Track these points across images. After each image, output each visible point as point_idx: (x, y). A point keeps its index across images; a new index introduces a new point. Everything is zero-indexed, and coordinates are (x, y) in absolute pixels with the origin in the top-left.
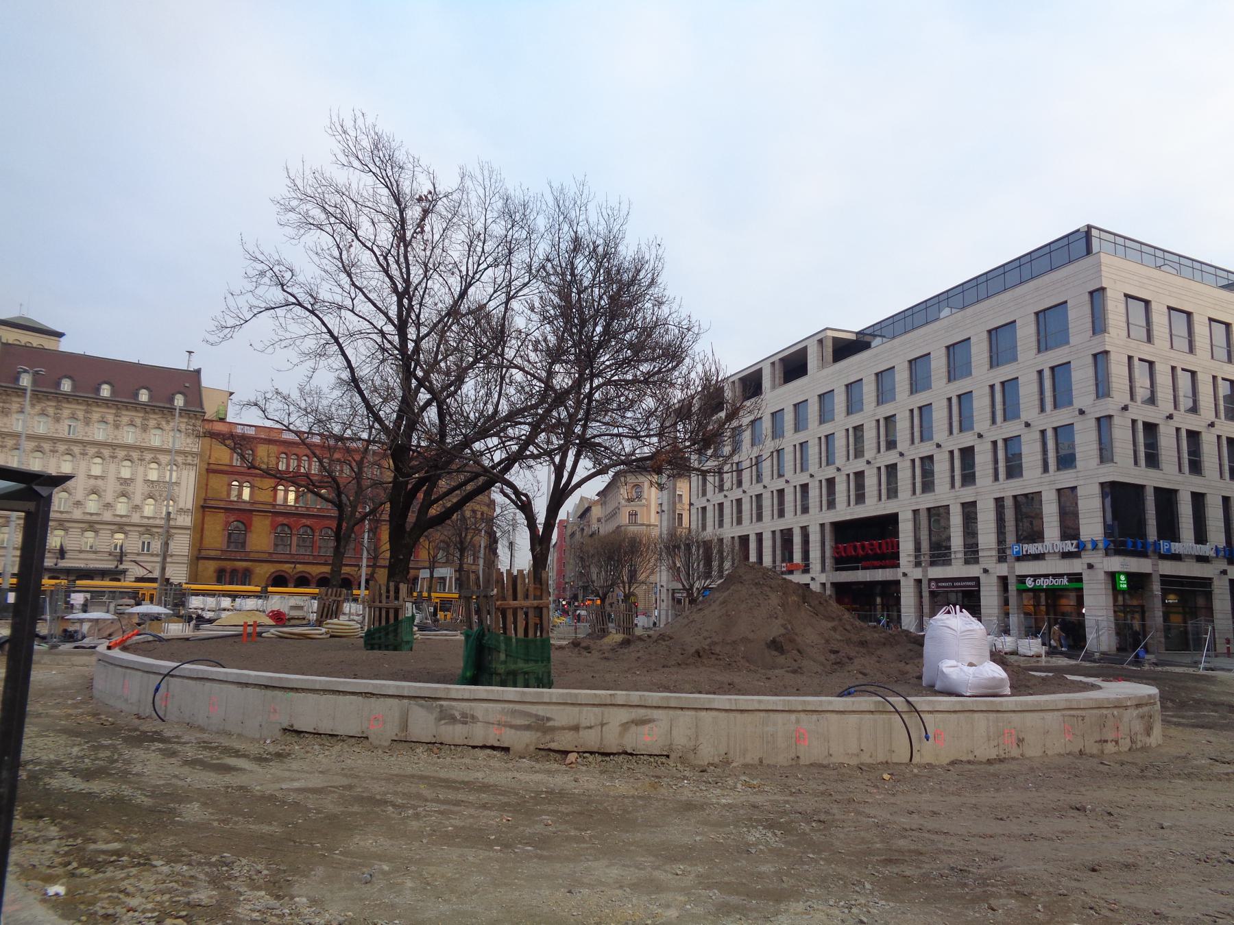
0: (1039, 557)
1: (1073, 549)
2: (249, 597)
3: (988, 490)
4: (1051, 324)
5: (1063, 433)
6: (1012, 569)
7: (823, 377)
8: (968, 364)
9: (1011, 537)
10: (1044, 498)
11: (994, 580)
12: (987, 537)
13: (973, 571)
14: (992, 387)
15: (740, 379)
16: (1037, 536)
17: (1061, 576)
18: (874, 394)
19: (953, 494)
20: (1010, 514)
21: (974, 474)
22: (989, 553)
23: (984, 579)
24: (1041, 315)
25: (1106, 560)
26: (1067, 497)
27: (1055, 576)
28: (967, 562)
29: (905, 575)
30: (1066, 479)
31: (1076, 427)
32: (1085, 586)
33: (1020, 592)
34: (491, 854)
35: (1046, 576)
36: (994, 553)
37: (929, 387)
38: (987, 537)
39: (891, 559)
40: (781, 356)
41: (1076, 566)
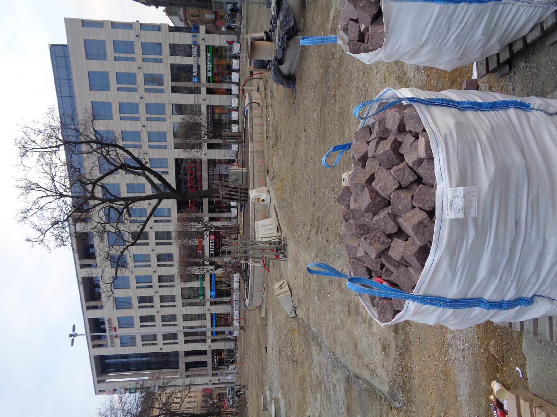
0: (199, 67)
1: (196, 47)
2: (422, 100)
3: (179, 310)
4: (98, 81)
5: (164, 318)
6: (208, 300)
7: (104, 272)
8: (125, 298)
9: (190, 85)
10: (185, 313)
11: (209, 96)
12: (196, 310)
13: (208, 317)
14: (143, 345)
15: (80, 259)
16: (189, 69)
17: (207, 56)
18: (128, 329)
19: (177, 286)
20: (189, 301)
21: (168, 254)
22: (196, 98)
23: (213, 348)
24: (118, 307)
25: (201, 32)
26: (186, 318)
27: (207, 60)
28: (205, 319)
29: (210, 347)
30: (180, 318)
31: (143, 41)
32: (211, 45)
33: (214, 82)
34: (463, 379)
35: (207, 64)
36: (202, 307)
37: (118, 185)
38: (196, 310)
39: (197, 163)
40: (95, 376)
41: (203, 48)
